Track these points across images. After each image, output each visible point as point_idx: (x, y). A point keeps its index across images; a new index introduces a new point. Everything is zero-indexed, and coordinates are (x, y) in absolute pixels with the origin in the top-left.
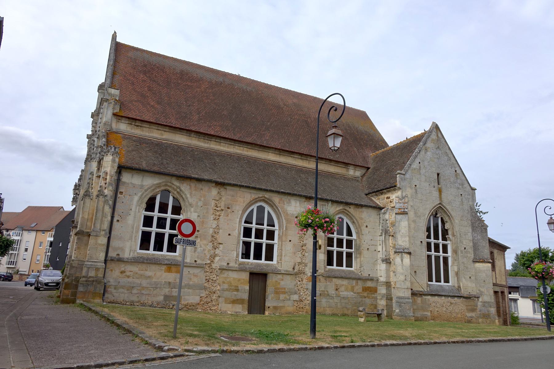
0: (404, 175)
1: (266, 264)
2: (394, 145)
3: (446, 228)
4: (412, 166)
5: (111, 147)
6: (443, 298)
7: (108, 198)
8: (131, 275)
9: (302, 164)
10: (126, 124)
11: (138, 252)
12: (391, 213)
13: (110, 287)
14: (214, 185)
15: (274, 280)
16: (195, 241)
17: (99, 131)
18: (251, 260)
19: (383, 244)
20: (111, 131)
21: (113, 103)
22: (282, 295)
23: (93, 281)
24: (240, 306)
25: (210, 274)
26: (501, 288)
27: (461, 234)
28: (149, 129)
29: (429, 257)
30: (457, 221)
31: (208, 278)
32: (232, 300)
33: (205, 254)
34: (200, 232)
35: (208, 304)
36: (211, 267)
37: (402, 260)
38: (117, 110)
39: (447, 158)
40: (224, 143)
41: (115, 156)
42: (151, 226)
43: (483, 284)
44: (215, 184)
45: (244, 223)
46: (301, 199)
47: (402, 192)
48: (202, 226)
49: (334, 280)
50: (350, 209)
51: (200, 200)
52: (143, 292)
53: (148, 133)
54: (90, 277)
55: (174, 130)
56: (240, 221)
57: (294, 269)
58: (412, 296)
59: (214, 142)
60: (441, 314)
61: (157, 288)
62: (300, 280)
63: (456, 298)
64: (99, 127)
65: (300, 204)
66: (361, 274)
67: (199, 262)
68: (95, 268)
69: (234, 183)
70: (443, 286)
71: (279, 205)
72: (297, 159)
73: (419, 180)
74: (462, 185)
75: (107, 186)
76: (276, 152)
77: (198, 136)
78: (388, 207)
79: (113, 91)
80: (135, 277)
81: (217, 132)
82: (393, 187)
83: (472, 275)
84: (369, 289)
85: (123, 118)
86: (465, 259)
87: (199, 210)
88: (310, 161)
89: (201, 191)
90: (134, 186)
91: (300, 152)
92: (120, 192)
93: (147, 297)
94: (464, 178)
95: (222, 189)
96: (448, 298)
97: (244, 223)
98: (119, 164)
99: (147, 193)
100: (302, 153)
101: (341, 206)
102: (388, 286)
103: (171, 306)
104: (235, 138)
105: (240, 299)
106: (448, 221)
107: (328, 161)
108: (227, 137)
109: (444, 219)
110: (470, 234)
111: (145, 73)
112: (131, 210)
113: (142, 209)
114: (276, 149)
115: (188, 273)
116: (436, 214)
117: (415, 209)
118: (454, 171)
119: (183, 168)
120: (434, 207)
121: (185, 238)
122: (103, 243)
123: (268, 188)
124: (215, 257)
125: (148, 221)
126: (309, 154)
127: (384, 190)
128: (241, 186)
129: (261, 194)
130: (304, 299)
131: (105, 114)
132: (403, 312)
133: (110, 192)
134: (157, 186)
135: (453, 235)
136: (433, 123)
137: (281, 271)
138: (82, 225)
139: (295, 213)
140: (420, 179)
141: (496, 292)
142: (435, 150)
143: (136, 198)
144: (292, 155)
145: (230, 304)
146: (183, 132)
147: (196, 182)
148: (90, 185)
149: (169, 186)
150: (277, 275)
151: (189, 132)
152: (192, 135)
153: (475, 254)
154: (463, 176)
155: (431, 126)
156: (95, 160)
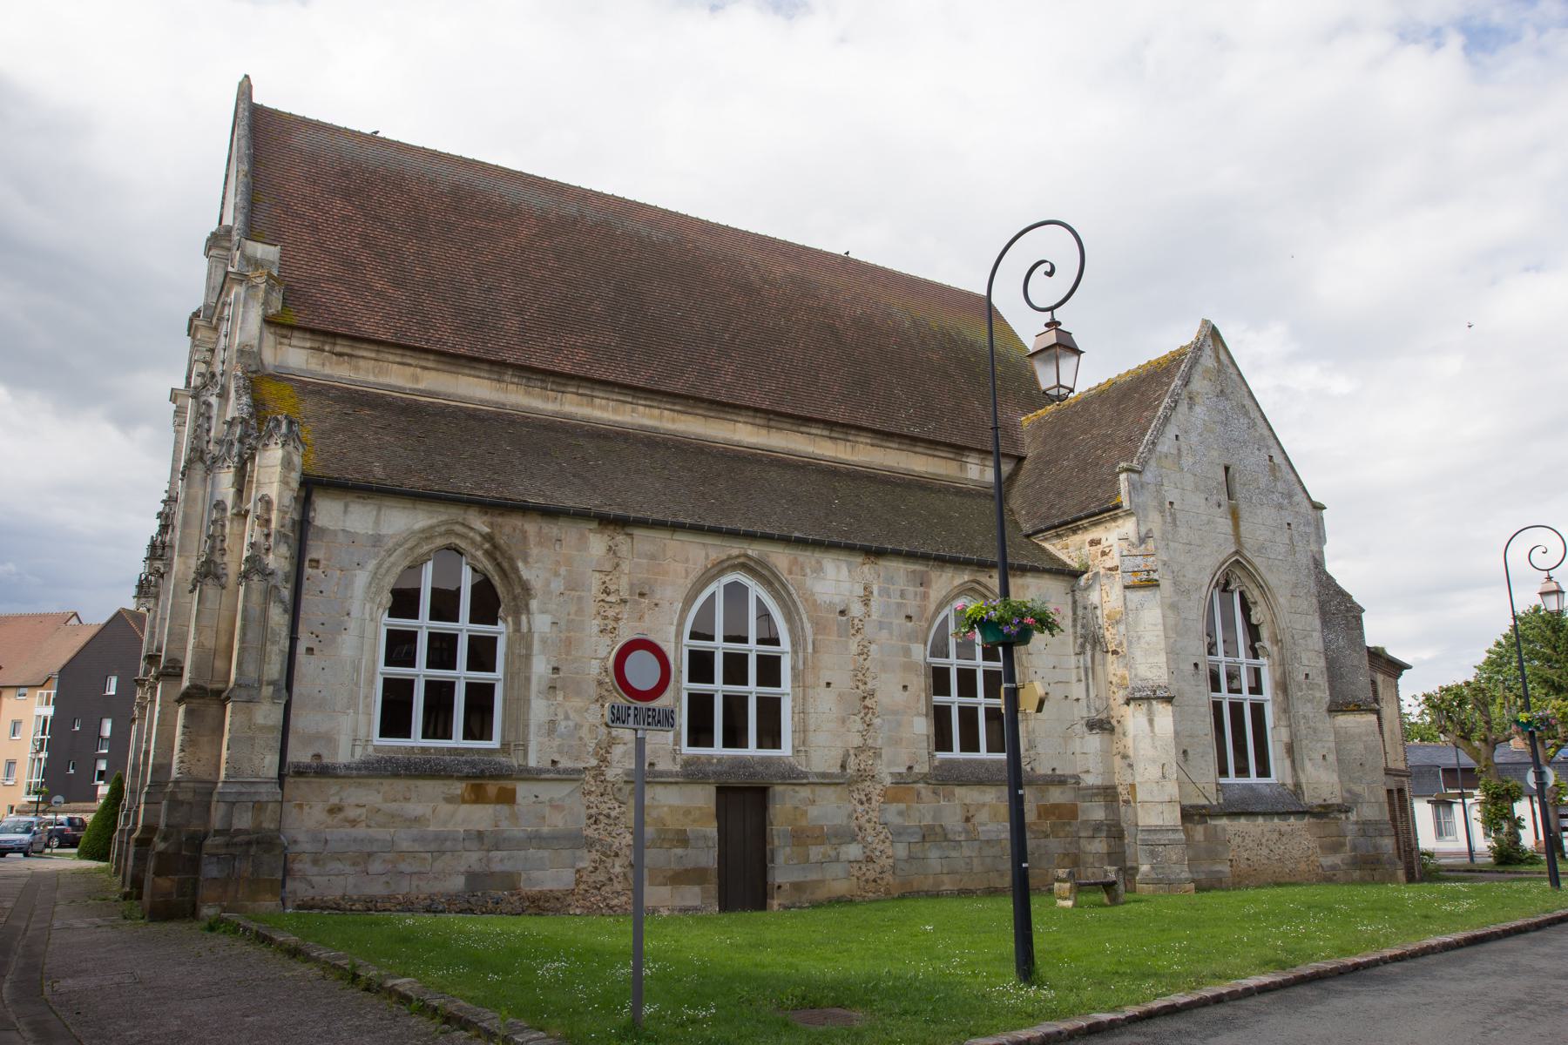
0: (1139, 472)
1: (763, 758)
2: (1089, 390)
3: (1254, 621)
4: (1159, 448)
5: (277, 420)
6: (1260, 820)
7: (278, 580)
8: (360, 816)
9: (834, 455)
10: (305, 352)
11: (375, 743)
12: (1107, 588)
13: (299, 858)
14: (594, 525)
15: (789, 806)
16: (672, 711)
17: (222, 375)
18: (718, 750)
19: (1087, 679)
20: (260, 374)
21: (263, 286)
22: (814, 847)
23: (249, 843)
24: (697, 889)
25: (600, 799)
26: (1396, 778)
27: (1296, 637)
28: (376, 363)
29: (1217, 706)
30: (1282, 600)
31: (593, 811)
32: (670, 873)
33: (581, 739)
34: (561, 674)
35: (599, 889)
36: (603, 778)
37: (1151, 722)
38: (276, 304)
39: (1246, 421)
40: (603, 398)
41: (290, 448)
42: (452, 665)
43: (1360, 774)
44: (600, 524)
45: (691, 638)
46: (851, 559)
47: (1138, 524)
48: (568, 653)
49: (959, 791)
50: (992, 580)
51: (557, 574)
52: (403, 867)
53: (375, 376)
54: (239, 832)
55: (449, 364)
56: (679, 634)
57: (843, 767)
58: (1183, 824)
59: (574, 396)
60: (1256, 866)
61: (444, 852)
62: (864, 799)
63: (1292, 819)
64: (223, 363)
65: (849, 571)
66: (1032, 769)
67: (565, 763)
68: (251, 804)
69: (655, 516)
70: (1255, 786)
71: (789, 577)
72: (817, 439)
73: (1179, 486)
74: (1290, 496)
75: (272, 544)
76: (758, 421)
77: (524, 381)
78: (1095, 570)
79: (260, 250)
80: (373, 824)
81: (581, 366)
82: (1108, 511)
83: (1329, 748)
84: (1057, 812)
85: (297, 334)
86: (1309, 705)
87: (554, 606)
88: (857, 442)
89: (557, 547)
90: (352, 538)
91: (827, 418)
92: (310, 561)
93: (414, 883)
94: (1292, 476)
95: (620, 538)
96: (1272, 820)
97: (691, 638)
98: (303, 474)
99: (392, 559)
100: (834, 419)
101: (967, 572)
102: (1109, 799)
103: (490, 905)
104: (635, 383)
105: (695, 870)
106: (1260, 600)
107: (907, 442)
108: (611, 378)
109: (1248, 595)
110: (1317, 635)
111: (347, 196)
112: (348, 614)
113: (381, 610)
114: (756, 410)
115: (535, 799)
116: (1227, 583)
117: (1173, 572)
118: (1267, 458)
119: (496, 476)
120: (1223, 563)
121: (640, 704)
122: (270, 723)
123: (755, 528)
124: (610, 747)
125: (400, 648)
126: (852, 422)
127: (1081, 519)
128: (676, 527)
129: (735, 549)
130: (878, 853)
131: (239, 322)
132: (1160, 870)
133: (283, 560)
134: (421, 535)
135: (1276, 641)
136: (1206, 322)
137: (807, 777)
138: (197, 667)
139: (837, 599)
140: (1182, 483)
141: (1389, 792)
142: (1215, 399)
143: (361, 578)
144: (803, 429)
145: (666, 885)
146: (480, 369)
147: (539, 520)
148: (214, 541)
149: (458, 535)
150: (797, 788)
151: (497, 367)
152: (507, 378)
153: (1332, 688)
154: (1290, 471)
155: (1200, 332)
156: (226, 465)
